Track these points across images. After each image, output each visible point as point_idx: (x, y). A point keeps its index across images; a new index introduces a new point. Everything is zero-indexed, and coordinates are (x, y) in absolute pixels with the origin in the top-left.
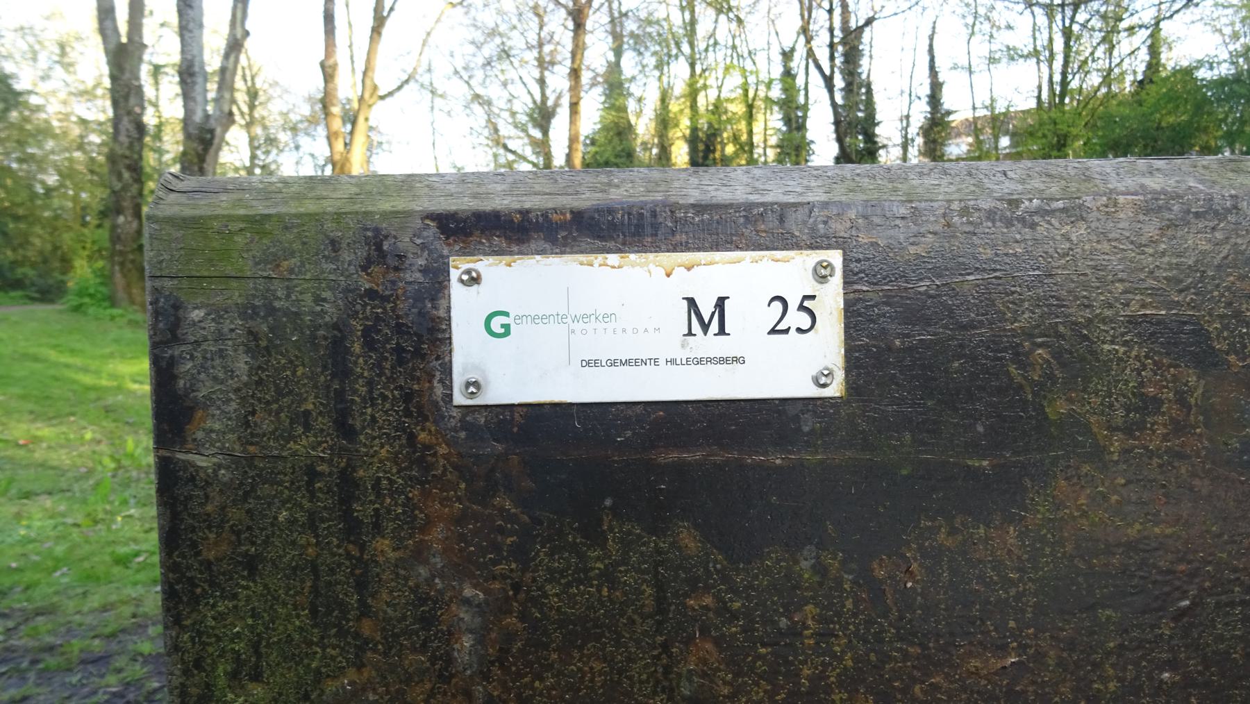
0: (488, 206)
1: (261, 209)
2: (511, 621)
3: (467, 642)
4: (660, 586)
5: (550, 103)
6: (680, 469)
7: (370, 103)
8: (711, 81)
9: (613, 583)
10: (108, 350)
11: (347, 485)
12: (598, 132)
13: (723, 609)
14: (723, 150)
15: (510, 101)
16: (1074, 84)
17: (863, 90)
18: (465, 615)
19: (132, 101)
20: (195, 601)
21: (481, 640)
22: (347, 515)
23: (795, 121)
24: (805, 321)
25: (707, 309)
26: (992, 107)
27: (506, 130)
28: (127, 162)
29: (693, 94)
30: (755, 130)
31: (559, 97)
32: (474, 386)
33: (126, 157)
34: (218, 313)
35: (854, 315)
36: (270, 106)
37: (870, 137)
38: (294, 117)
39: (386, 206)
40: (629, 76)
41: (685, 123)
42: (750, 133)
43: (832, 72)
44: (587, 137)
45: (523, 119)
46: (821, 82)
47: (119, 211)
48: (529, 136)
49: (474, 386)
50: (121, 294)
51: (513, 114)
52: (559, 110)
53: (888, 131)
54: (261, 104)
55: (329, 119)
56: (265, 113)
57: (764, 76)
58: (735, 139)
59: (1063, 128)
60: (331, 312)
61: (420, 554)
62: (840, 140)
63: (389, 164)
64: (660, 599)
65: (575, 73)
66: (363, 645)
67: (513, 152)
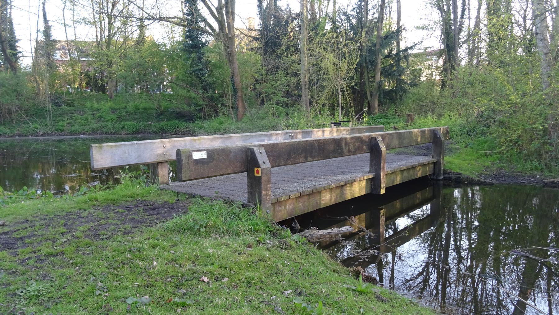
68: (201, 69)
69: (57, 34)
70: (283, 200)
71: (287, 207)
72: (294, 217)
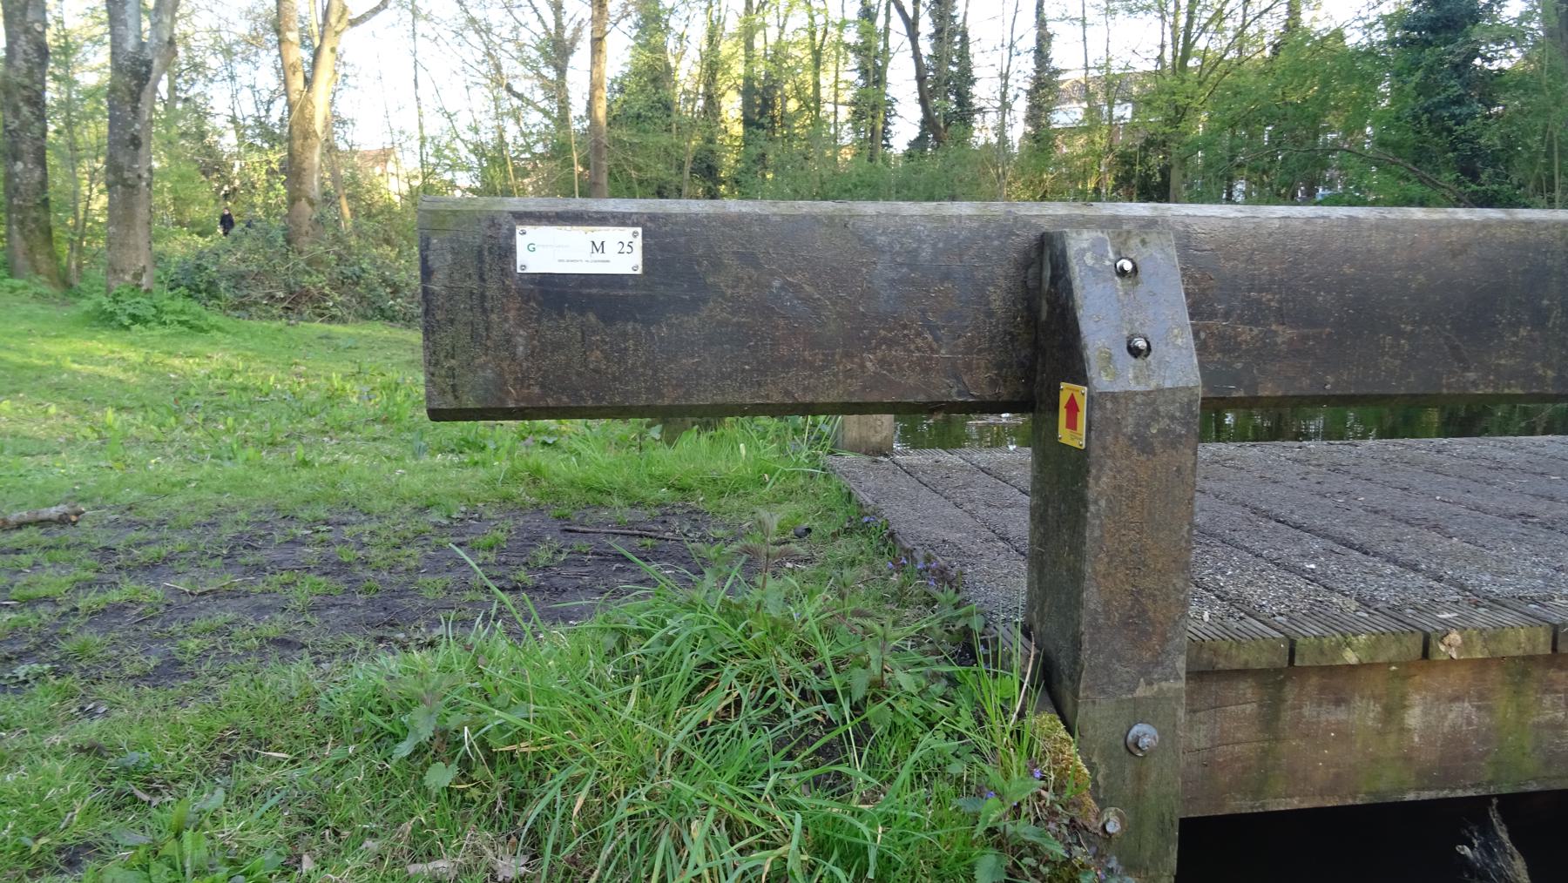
0: (528, 210)
1: (455, 208)
2: (535, 342)
3: (521, 348)
4: (583, 333)
5: (568, 34)
6: (589, 296)
7: (338, 29)
8: (771, 19)
9: (568, 331)
10: (22, 327)
11: (483, 297)
12: (628, 75)
13: (603, 341)
14: (784, 105)
15: (515, 28)
16: (1201, 44)
17: (958, 38)
18: (519, 339)
19: (31, 16)
20: (434, 332)
21: (526, 347)
22: (483, 307)
23: (874, 74)
24: (629, 250)
25: (598, 245)
26: (1107, 65)
27: (510, 67)
28: (25, 93)
29: (748, 35)
30: (823, 82)
31: (578, 30)
32: (523, 267)
33: (25, 87)
34: (441, 241)
35: (645, 248)
36: (195, 20)
37: (963, 99)
38: (227, 38)
39: (495, 208)
40: (669, 6)
41: (738, 69)
42: (817, 85)
43: (916, 12)
44: (614, 81)
45: (535, 54)
46: (903, 30)
47: (16, 157)
48: (540, 76)
49: (523, 267)
50: (21, 261)
51: (520, 48)
52: (578, 44)
53: (984, 91)
54: (182, 16)
55: (284, 47)
56: (190, 31)
57: (836, 16)
58: (799, 92)
59: (1181, 101)
60: (478, 241)
61: (506, 320)
62: (923, 101)
63: (1027, 535)
64: (583, 337)
65: (448, 637)
66: (488, 348)
67: (519, 96)
68: (1459, 101)
69: (1067, 57)
70: (1351, 657)
71: (1414, 717)
72: (1484, 800)
